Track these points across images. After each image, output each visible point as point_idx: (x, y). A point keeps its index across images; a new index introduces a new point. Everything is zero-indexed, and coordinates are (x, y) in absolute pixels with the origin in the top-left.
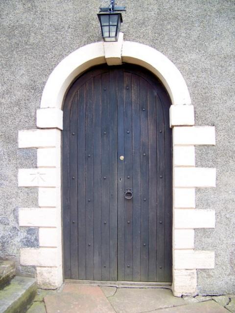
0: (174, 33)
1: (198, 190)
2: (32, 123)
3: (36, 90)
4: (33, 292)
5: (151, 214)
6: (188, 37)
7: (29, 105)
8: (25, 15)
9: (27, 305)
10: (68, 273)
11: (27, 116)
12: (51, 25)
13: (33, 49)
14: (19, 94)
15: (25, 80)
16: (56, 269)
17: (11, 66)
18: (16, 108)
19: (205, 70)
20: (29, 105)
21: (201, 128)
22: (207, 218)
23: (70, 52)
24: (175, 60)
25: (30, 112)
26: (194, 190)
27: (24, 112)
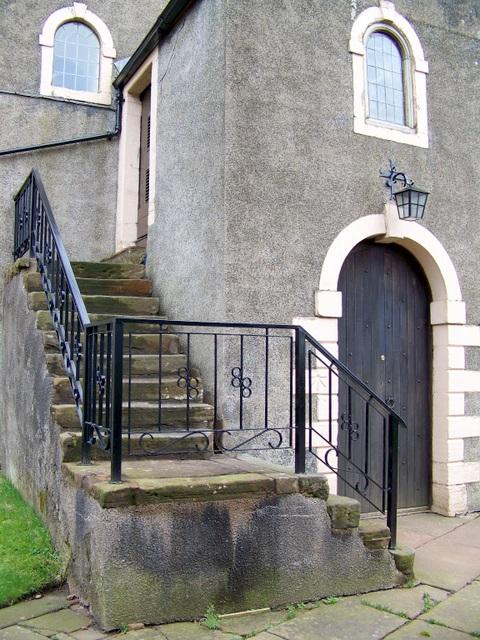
0: (446, 217)
1: (467, 394)
2: (308, 309)
3: (315, 265)
4: (413, 577)
5: (410, 341)
6: (459, 224)
7: (305, 284)
8: (299, 158)
9: (118, 500)
10: (338, 493)
11: (303, 299)
12: (328, 180)
13: (308, 207)
14: (292, 267)
15: (299, 249)
16: (292, 466)
17: (282, 226)
18: (289, 287)
19: (471, 264)
20: (305, 284)
21: (469, 418)
22: (471, 426)
23: (350, 221)
24: (448, 248)
25: (306, 294)
26: (463, 395)
27: (299, 292)
